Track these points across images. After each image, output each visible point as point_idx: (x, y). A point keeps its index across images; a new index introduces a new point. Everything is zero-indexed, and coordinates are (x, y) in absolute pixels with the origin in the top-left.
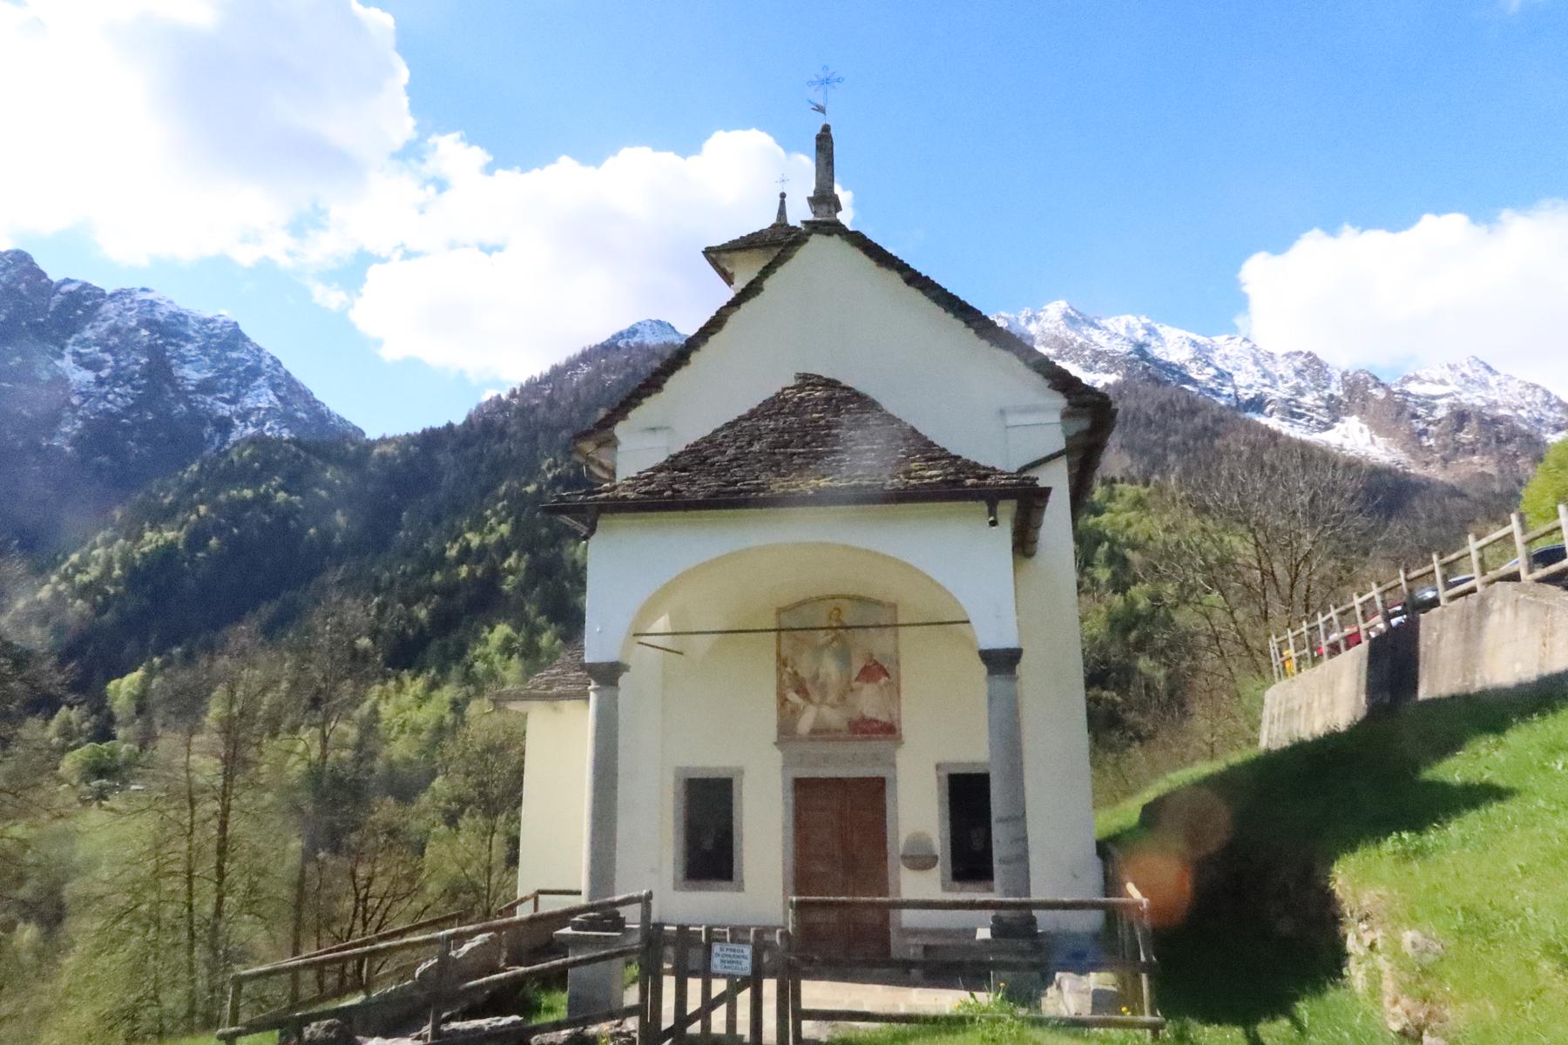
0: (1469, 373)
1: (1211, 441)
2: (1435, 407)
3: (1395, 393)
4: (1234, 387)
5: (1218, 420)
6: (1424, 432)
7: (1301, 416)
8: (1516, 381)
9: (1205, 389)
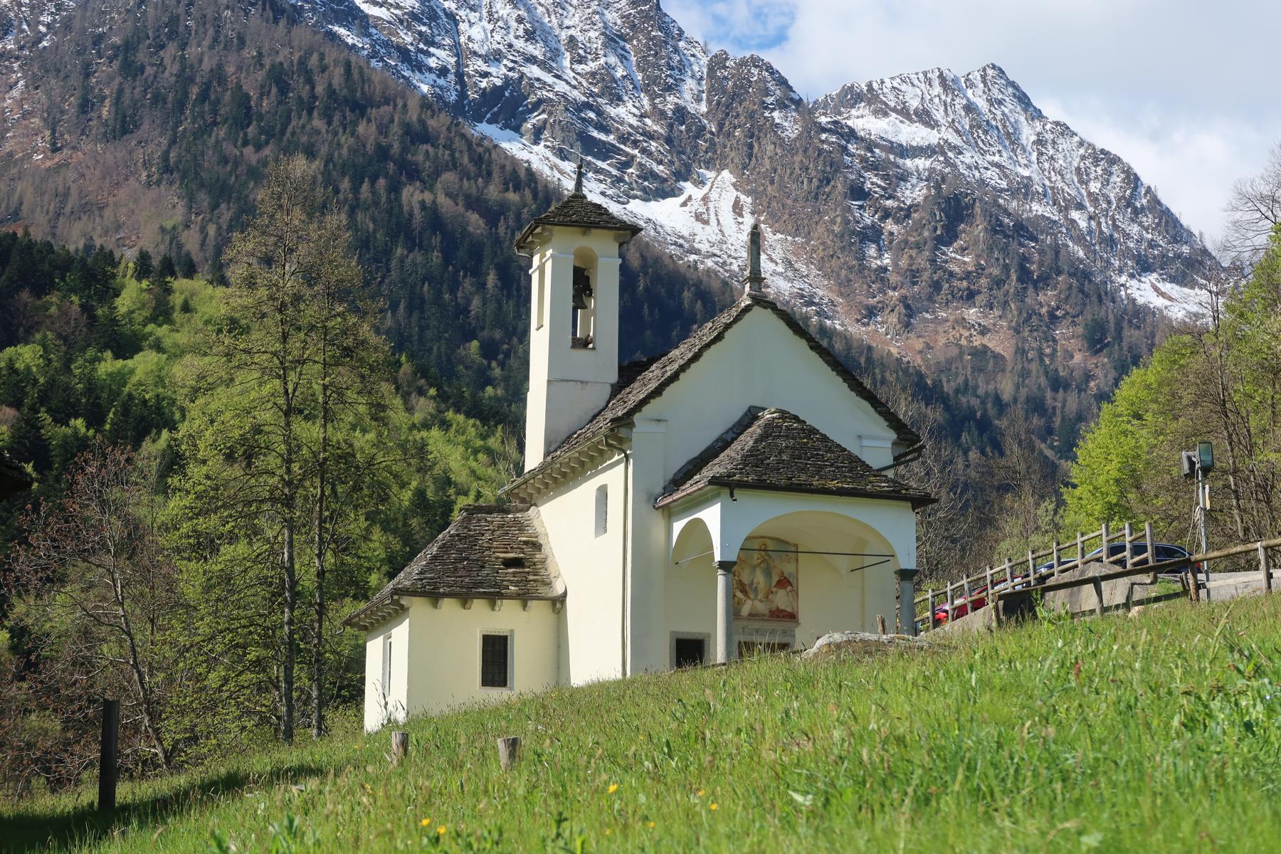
0: (982, 104)
1: (395, 188)
2: (904, 177)
3: (824, 130)
4: (457, 50)
5: (417, 135)
6: (873, 235)
7: (605, 151)
8: (1076, 139)
9: (387, 44)
